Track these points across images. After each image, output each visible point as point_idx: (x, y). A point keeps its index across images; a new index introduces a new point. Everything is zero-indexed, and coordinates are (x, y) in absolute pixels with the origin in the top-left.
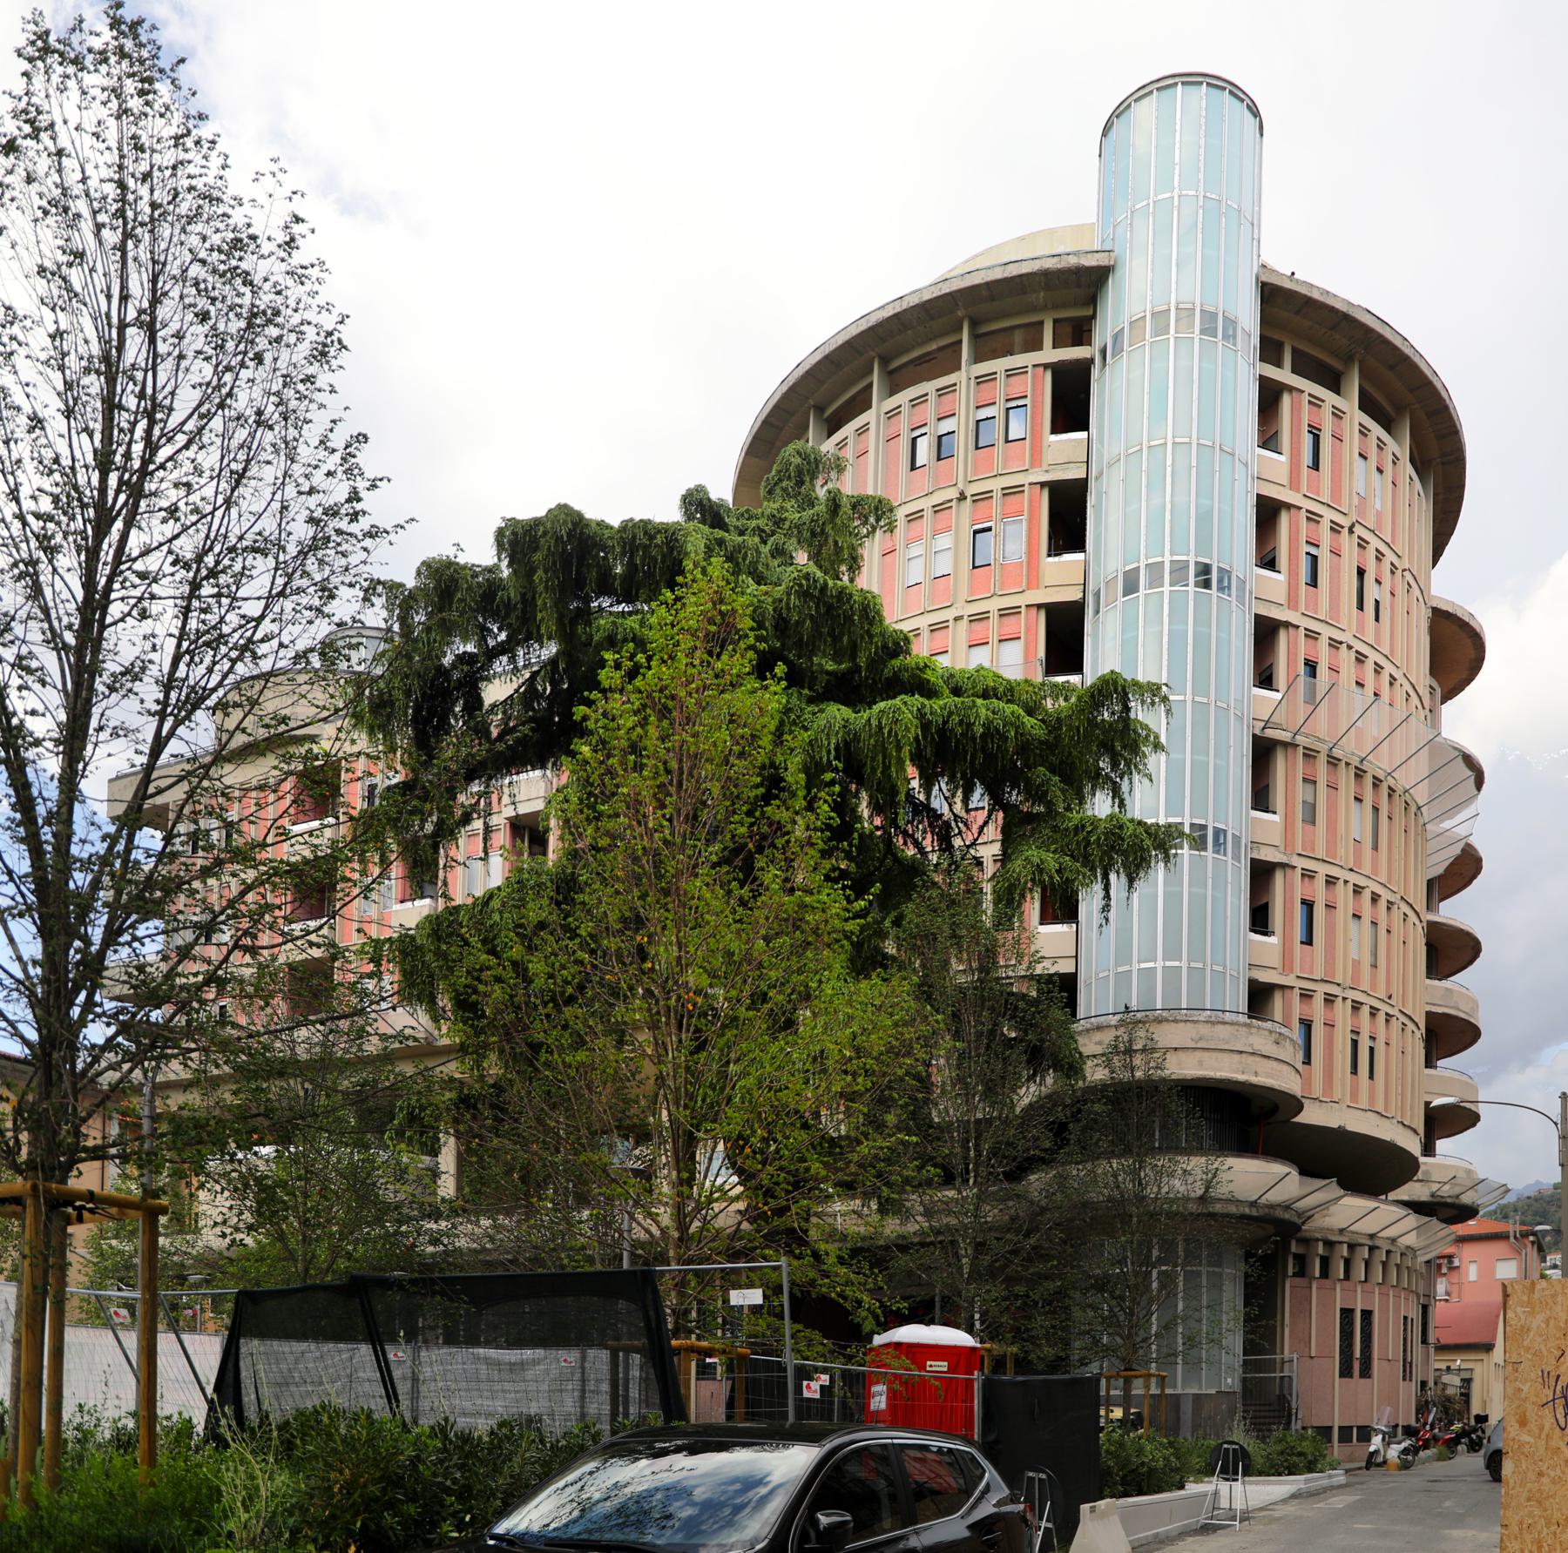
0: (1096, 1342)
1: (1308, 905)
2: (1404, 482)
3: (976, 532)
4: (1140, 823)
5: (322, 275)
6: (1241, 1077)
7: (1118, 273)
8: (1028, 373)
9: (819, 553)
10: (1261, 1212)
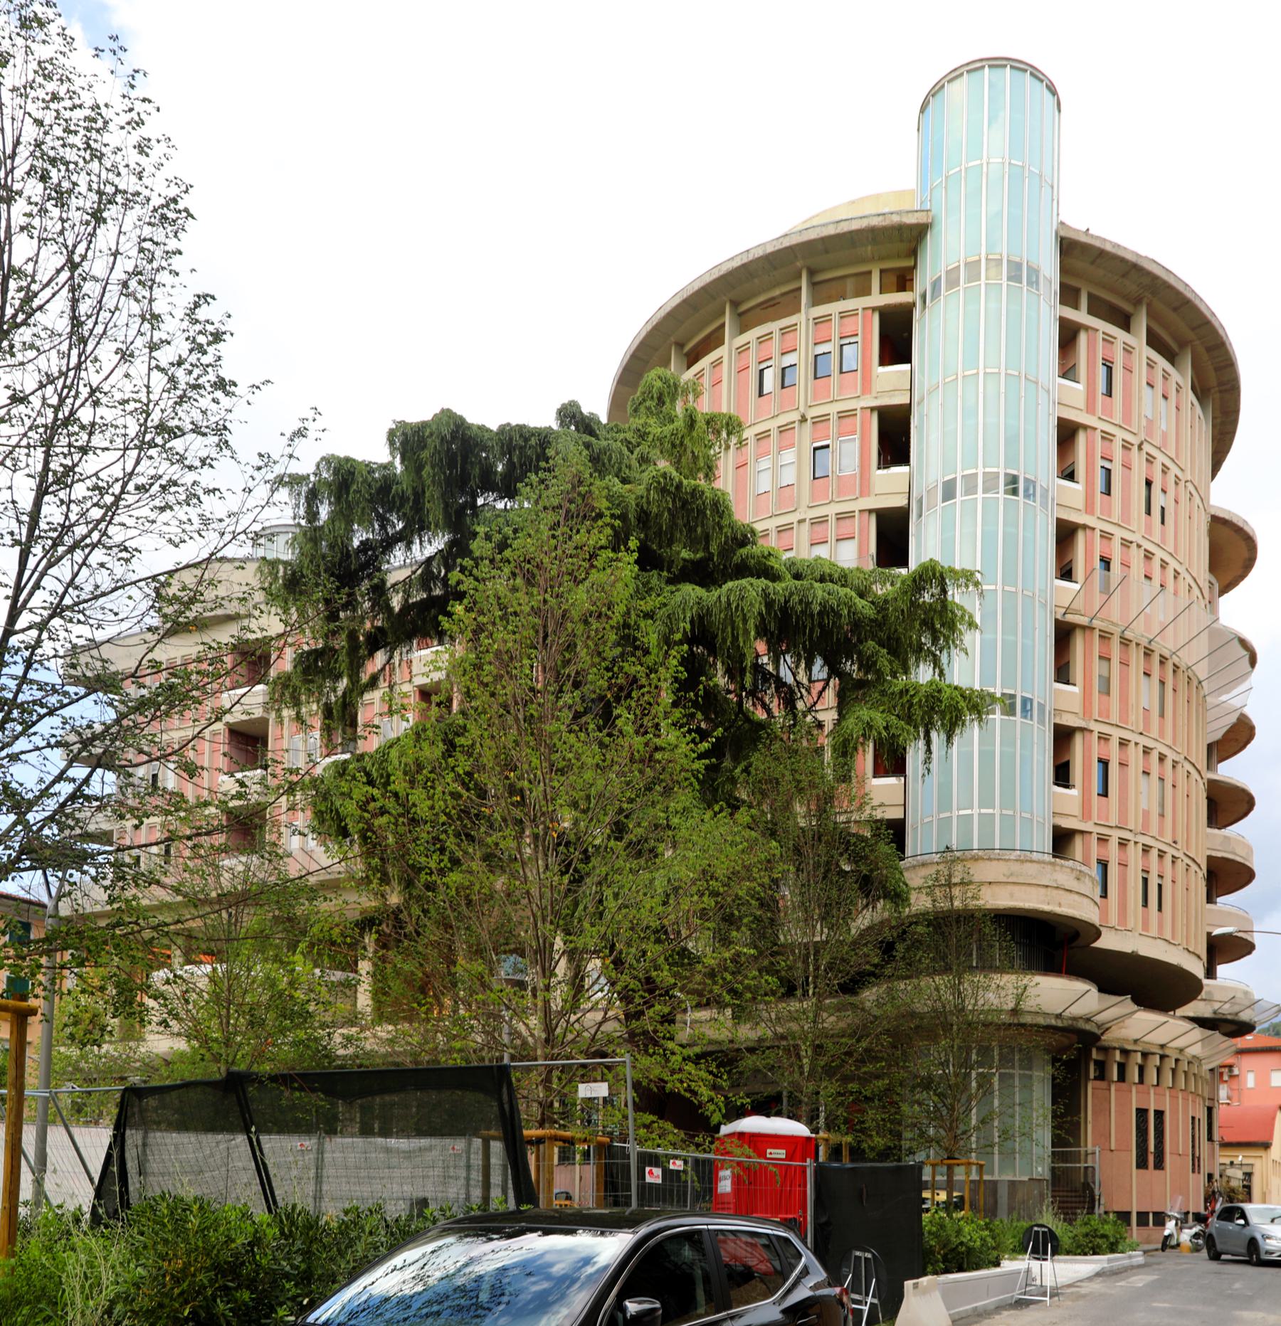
0: (922, 1134)
1: (1104, 763)
2: (1186, 408)
3: (815, 449)
4: (956, 688)
5: (169, 151)
6: (1047, 908)
7: (935, 230)
8: (859, 313)
9: (679, 462)
10: (1066, 1024)
